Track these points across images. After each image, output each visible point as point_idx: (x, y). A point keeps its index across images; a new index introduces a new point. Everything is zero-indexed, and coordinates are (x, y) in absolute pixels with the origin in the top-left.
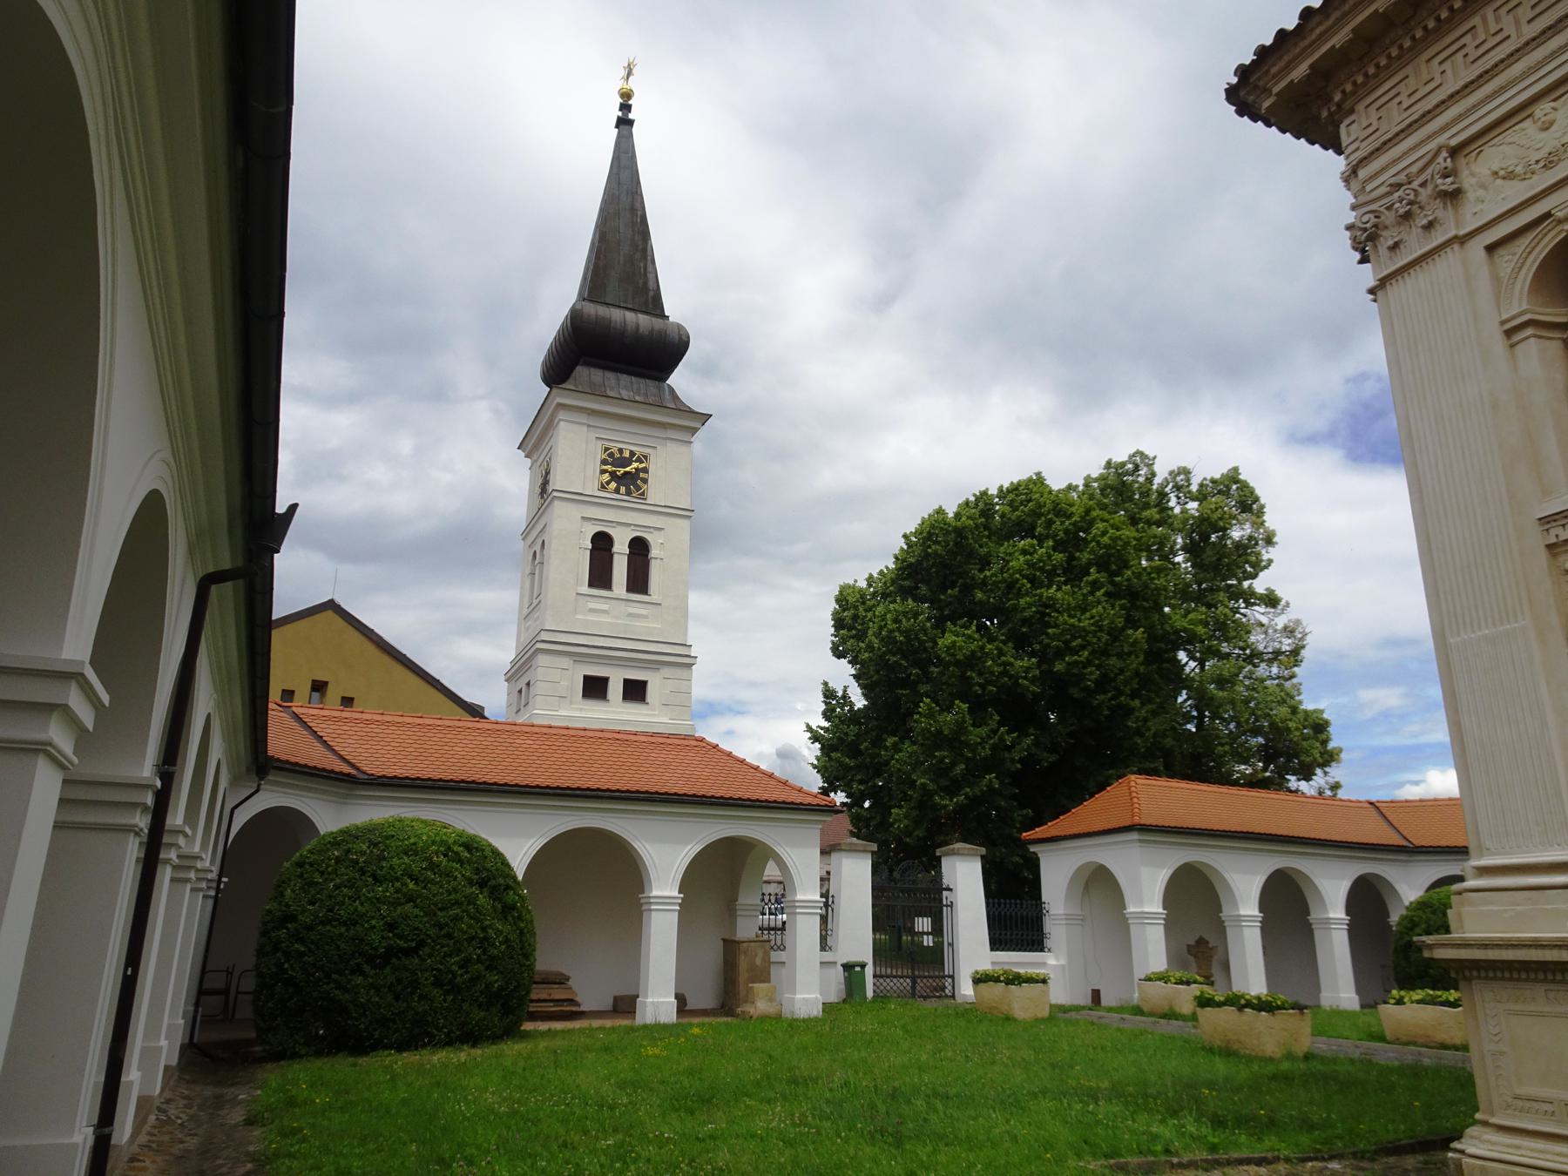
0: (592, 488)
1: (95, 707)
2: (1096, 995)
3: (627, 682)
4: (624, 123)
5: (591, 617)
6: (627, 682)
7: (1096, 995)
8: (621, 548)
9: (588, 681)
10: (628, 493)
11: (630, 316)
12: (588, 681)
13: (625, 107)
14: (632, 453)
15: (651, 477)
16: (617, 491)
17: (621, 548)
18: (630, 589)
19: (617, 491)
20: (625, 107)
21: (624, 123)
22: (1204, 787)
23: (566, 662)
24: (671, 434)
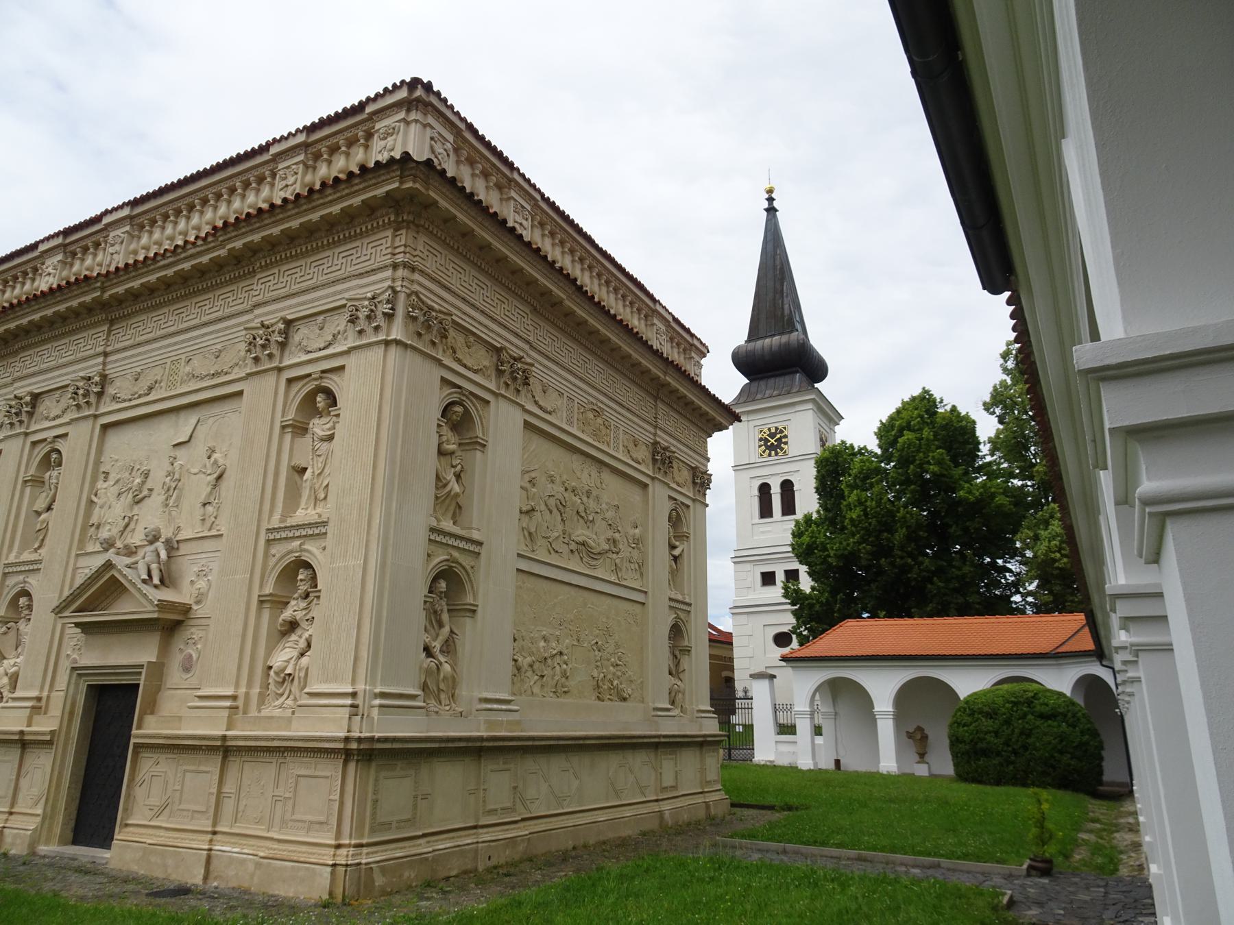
0: (755, 458)
1: (1091, 656)
2: (837, 762)
3: (787, 572)
4: (771, 210)
5: (762, 537)
6: (787, 572)
7: (837, 762)
8: (776, 490)
9: (764, 575)
10: (777, 454)
11: (768, 341)
12: (764, 575)
13: (770, 200)
14: (777, 428)
15: (790, 440)
16: (770, 455)
17: (776, 490)
18: (784, 514)
19: (770, 455)
20: (770, 200)
21: (771, 210)
22: (992, 619)
23: (748, 567)
24: (798, 408)
